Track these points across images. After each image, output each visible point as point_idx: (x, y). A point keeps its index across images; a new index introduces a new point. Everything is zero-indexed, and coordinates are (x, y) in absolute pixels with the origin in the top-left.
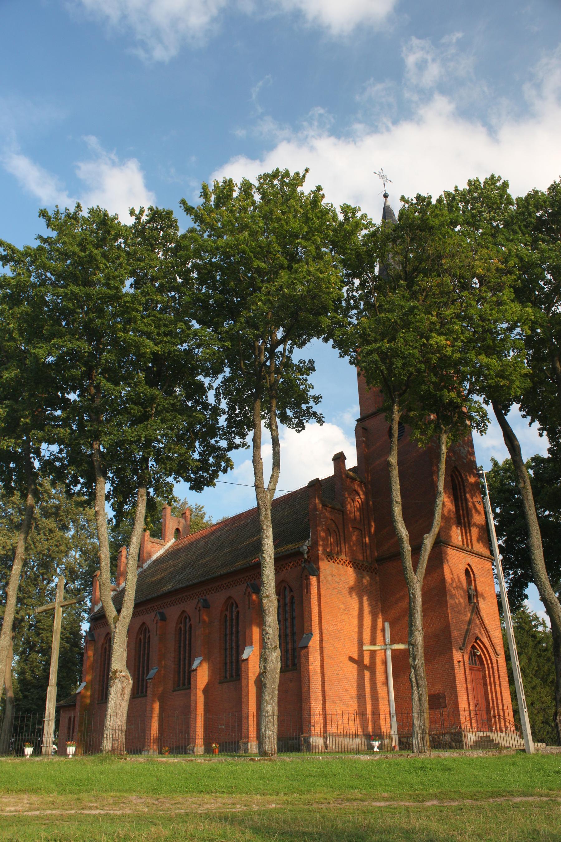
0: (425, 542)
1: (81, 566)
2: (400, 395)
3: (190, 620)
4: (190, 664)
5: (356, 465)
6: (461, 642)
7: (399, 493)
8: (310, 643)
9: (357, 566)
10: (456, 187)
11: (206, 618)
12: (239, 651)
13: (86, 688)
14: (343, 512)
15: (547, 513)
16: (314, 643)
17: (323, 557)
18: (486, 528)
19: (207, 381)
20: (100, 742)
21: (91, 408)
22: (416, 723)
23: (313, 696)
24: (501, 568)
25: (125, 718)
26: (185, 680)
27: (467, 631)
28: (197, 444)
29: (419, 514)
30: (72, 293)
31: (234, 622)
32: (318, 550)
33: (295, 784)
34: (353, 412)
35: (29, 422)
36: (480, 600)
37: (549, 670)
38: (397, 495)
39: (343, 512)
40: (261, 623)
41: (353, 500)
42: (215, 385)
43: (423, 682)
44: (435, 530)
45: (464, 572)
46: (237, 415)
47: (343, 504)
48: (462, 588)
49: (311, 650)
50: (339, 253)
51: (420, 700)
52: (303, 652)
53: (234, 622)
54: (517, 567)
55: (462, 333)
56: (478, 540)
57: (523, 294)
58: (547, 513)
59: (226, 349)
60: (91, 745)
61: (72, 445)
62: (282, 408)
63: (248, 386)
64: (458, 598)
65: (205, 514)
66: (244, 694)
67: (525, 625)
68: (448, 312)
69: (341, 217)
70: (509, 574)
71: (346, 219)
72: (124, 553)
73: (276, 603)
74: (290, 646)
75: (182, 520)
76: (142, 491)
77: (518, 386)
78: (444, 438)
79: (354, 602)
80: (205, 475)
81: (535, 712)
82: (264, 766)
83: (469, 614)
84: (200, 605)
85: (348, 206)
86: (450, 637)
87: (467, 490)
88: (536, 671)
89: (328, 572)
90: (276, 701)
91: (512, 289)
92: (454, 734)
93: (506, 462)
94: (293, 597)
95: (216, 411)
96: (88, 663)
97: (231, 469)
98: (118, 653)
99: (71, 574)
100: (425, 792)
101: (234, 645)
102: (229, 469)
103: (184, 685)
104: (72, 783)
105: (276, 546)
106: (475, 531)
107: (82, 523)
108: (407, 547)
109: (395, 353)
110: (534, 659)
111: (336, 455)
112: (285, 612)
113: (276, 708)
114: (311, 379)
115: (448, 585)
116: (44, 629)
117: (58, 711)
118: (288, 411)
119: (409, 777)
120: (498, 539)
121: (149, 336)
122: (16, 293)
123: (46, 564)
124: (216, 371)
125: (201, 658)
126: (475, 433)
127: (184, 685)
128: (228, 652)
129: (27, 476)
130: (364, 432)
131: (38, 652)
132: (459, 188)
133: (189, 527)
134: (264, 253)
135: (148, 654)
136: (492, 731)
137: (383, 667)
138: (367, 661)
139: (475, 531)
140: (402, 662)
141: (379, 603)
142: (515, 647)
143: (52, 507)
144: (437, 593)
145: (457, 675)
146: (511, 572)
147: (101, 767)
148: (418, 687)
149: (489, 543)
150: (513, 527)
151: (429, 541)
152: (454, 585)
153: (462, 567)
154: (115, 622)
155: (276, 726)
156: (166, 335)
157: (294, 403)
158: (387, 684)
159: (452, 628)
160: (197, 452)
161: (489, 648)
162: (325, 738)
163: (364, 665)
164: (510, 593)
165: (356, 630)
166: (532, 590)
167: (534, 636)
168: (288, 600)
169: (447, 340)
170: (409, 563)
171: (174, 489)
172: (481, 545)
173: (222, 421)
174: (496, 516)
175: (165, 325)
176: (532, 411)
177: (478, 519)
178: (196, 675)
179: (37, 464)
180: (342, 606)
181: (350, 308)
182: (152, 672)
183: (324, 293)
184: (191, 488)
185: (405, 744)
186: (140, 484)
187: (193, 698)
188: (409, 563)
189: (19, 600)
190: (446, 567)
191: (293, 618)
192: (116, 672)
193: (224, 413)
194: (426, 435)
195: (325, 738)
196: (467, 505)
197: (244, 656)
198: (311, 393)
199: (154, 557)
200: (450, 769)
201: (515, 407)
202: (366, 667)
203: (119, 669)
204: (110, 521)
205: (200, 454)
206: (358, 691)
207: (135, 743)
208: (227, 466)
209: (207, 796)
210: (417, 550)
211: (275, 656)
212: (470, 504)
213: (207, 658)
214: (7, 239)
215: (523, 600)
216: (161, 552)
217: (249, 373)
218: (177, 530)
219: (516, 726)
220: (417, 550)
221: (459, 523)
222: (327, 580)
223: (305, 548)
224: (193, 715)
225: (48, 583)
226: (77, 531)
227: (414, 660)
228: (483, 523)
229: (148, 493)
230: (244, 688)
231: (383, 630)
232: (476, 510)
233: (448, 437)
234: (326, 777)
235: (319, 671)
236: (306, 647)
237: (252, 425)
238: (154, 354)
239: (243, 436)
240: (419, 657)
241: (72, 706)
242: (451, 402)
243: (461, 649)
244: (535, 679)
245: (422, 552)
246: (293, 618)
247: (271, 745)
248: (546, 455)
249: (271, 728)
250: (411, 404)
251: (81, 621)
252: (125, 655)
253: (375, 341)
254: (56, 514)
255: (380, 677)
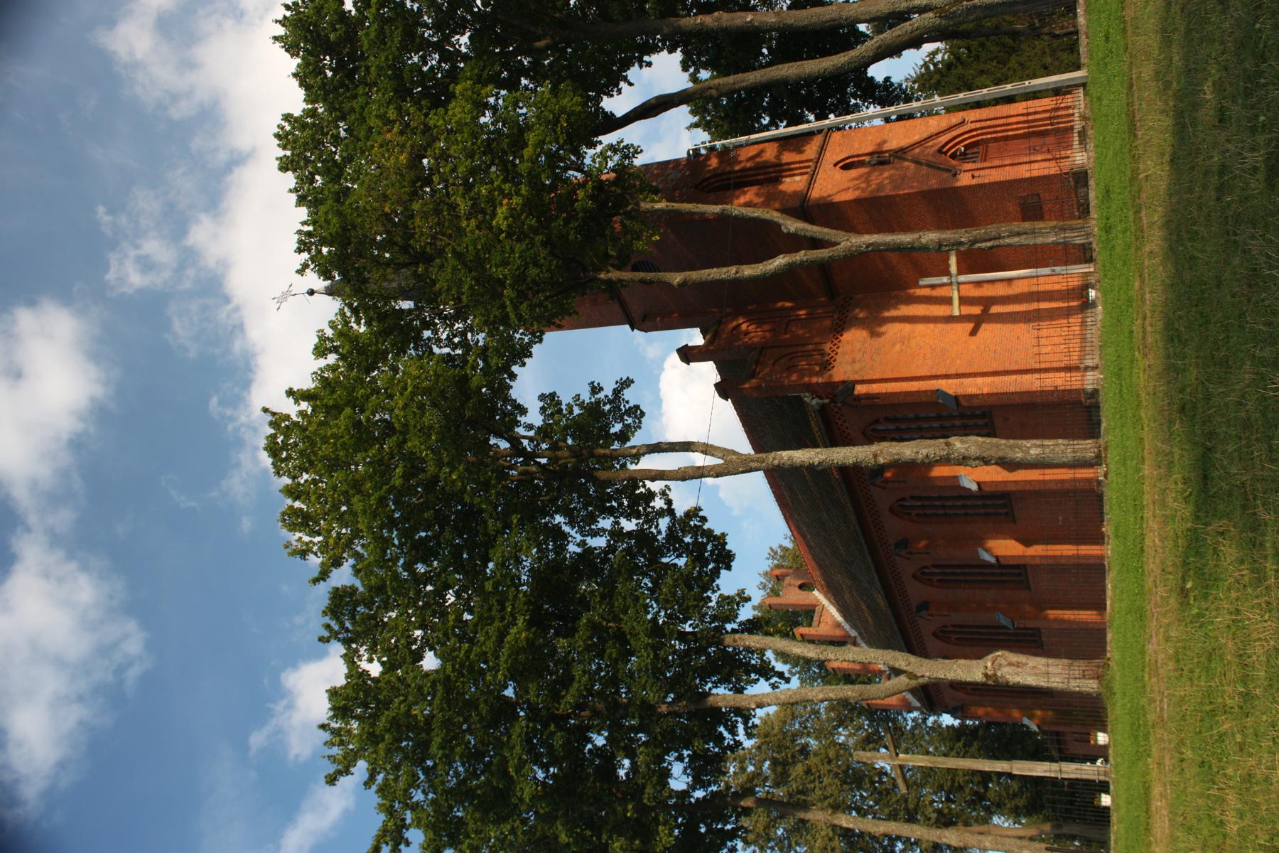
0: (792, 230)
1: (860, 727)
2: (585, 269)
3: (926, 567)
4: (989, 565)
5: (698, 330)
6: (946, 175)
7: (725, 269)
8: (951, 392)
9: (839, 328)
10: (290, 191)
11: (923, 543)
12: (966, 494)
13: (1031, 718)
14: (762, 349)
15: (765, 51)
16: (950, 387)
17: (826, 376)
18: (785, 142)
19: (572, 548)
20: (1081, 696)
21: (613, 717)
22: (1051, 239)
23: (1026, 387)
24: (848, 117)
25: (1051, 661)
26: (1014, 573)
27: (929, 165)
28: (665, 560)
29: (762, 239)
30: (441, 747)
31: (926, 503)
32: (817, 383)
33: (1130, 414)
34: (621, 333)
35: (644, 807)
36: (886, 147)
37: (997, 44)
38: (730, 272)
39: (762, 349)
40: (928, 464)
41: (747, 333)
42: (579, 538)
43: (992, 229)
44: (775, 216)
45: (845, 173)
46: (621, 504)
47: (751, 348)
48: (869, 174)
49: (961, 391)
50: (385, 360)
51: (1018, 234)
52: (963, 402)
53: (926, 503)
54: (844, 93)
55: (492, 182)
56: (801, 152)
57: (438, 95)
58: (765, 51)
59: (521, 523)
60: (1090, 712)
61: (668, 742)
62: (610, 438)
63: (582, 491)
64: (883, 180)
65: (780, 546)
66: (1028, 487)
67: (931, 80)
68: (463, 206)
69: (332, 359)
70: (856, 105)
71: (335, 350)
72: (836, 665)
73: (885, 445)
74: (958, 423)
75: (788, 580)
76: (728, 640)
77: (570, 101)
78: (645, 206)
79: (892, 330)
80: (709, 548)
81: (1057, 63)
82: (1113, 456)
83: (906, 163)
84: (903, 553)
85: (316, 348)
86: (938, 190)
87: (728, 169)
88: (999, 63)
89: (849, 368)
90: (1024, 442)
91: (432, 112)
92: (1077, 182)
93: (693, 112)
94: (886, 419)
95: (617, 534)
96: (996, 716)
97: (701, 510)
98: (959, 671)
99: (871, 742)
100: (1133, 229)
101: (959, 503)
102: (701, 514)
103: (1020, 574)
104: (1136, 738)
105: (815, 445)
106: (788, 157)
107: (797, 726)
108: (801, 256)
109: (520, 278)
110: (982, 66)
111: (682, 360)
112: (908, 430)
113: (1034, 441)
114: (566, 398)
115: (864, 195)
116: (953, 781)
117: (1072, 759)
118: (612, 431)
119: (1118, 249)
120: (808, 122)
121: (502, 635)
122: (444, 829)
123: (857, 778)
124: (559, 536)
125: (980, 550)
126: (639, 161)
127: (1020, 574)
128: (971, 511)
129: (717, 807)
130: (648, 318)
131: (987, 788)
132: (292, 186)
133: (798, 570)
134: (382, 468)
135: (978, 627)
136: (1072, 128)
137: (986, 286)
138: (976, 310)
139: (788, 157)
140: (975, 261)
141: (894, 293)
142: (961, 96)
143: (774, 771)
144: (875, 211)
145: (992, 179)
146: (853, 101)
147: (1118, 696)
148: (1000, 238)
149: (810, 134)
150: (790, 101)
151: (792, 225)
152: (863, 185)
153: (839, 175)
154: (916, 677)
155: (1060, 441)
156: (503, 608)
157: (600, 426)
158: (1009, 281)
159: (925, 188)
160: (676, 561)
161: (954, 133)
162: (1086, 368)
163: (983, 314)
164: (883, 104)
165: (931, 326)
166: (877, 72)
167: (949, 66)
168: (891, 427)
169: (501, 204)
170: (824, 253)
171: (726, 594)
172: (807, 148)
173: (629, 525)
174: (773, 124)
175: (490, 609)
176: (612, 81)
177: (770, 153)
178: (1004, 557)
179: (699, 794)
180: (898, 347)
181: (464, 344)
182: (1004, 621)
183: (437, 382)
184: (729, 568)
185: (1084, 254)
186: (719, 643)
187: (1038, 561)
188: (824, 253)
189: (911, 819)
190: (838, 198)
191: (917, 419)
192: (986, 675)
193: (618, 523)
194: (641, 231)
195: (1086, 368)
196: (750, 169)
197: (974, 487)
198: (586, 397)
199: (839, 618)
200: (1108, 191)
201: (608, 104)
202: (985, 311)
203: (982, 670)
204: (774, 686)
205: (679, 556)
206: (1019, 322)
207: (1086, 645)
208: (697, 515)
209: (1147, 540)
210: (816, 243)
211: (959, 445)
212: (749, 165)
213: (980, 541)
214: (369, 843)
215: (892, 84)
216: (833, 611)
217: (559, 489)
218: (801, 587)
219: (1065, 94)
220: (816, 243)
221: (777, 180)
222: (861, 369)
223: (814, 402)
224: (1063, 561)
225: (886, 774)
226: (808, 735)
227: (961, 243)
228: (775, 145)
229: (734, 631)
230: (1020, 488)
231: (933, 287)
232: (759, 155)
233: (644, 200)
234: (1121, 369)
235: (991, 379)
236: (956, 398)
237: (634, 481)
238: (529, 624)
239: (651, 495)
240: (957, 236)
241: (1058, 738)
242: (592, 197)
243: (955, 175)
244: (1010, 65)
245: (808, 234)
246: (917, 419)
247: (1086, 448)
248: (678, 56)
249: (1061, 448)
250: (602, 252)
251: (940, 726)
252: (962, 662)
253: (503, 307)
254: (785, 764)
255: (1000, 290)
